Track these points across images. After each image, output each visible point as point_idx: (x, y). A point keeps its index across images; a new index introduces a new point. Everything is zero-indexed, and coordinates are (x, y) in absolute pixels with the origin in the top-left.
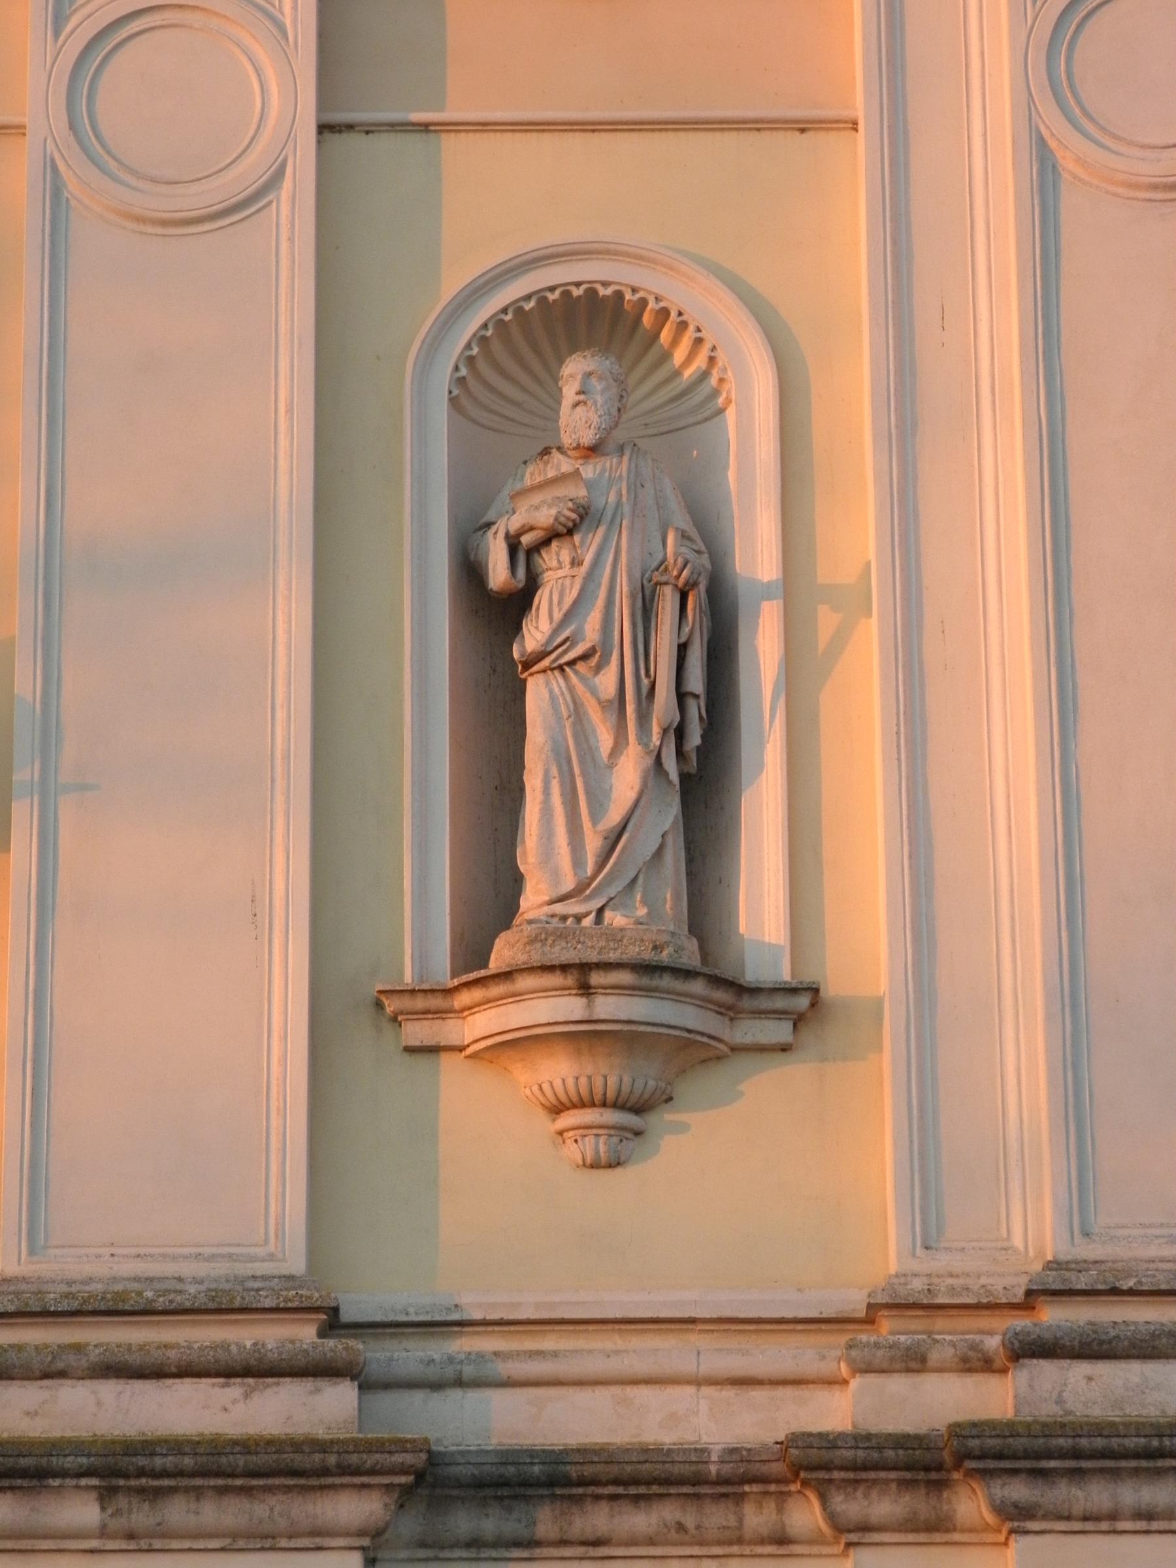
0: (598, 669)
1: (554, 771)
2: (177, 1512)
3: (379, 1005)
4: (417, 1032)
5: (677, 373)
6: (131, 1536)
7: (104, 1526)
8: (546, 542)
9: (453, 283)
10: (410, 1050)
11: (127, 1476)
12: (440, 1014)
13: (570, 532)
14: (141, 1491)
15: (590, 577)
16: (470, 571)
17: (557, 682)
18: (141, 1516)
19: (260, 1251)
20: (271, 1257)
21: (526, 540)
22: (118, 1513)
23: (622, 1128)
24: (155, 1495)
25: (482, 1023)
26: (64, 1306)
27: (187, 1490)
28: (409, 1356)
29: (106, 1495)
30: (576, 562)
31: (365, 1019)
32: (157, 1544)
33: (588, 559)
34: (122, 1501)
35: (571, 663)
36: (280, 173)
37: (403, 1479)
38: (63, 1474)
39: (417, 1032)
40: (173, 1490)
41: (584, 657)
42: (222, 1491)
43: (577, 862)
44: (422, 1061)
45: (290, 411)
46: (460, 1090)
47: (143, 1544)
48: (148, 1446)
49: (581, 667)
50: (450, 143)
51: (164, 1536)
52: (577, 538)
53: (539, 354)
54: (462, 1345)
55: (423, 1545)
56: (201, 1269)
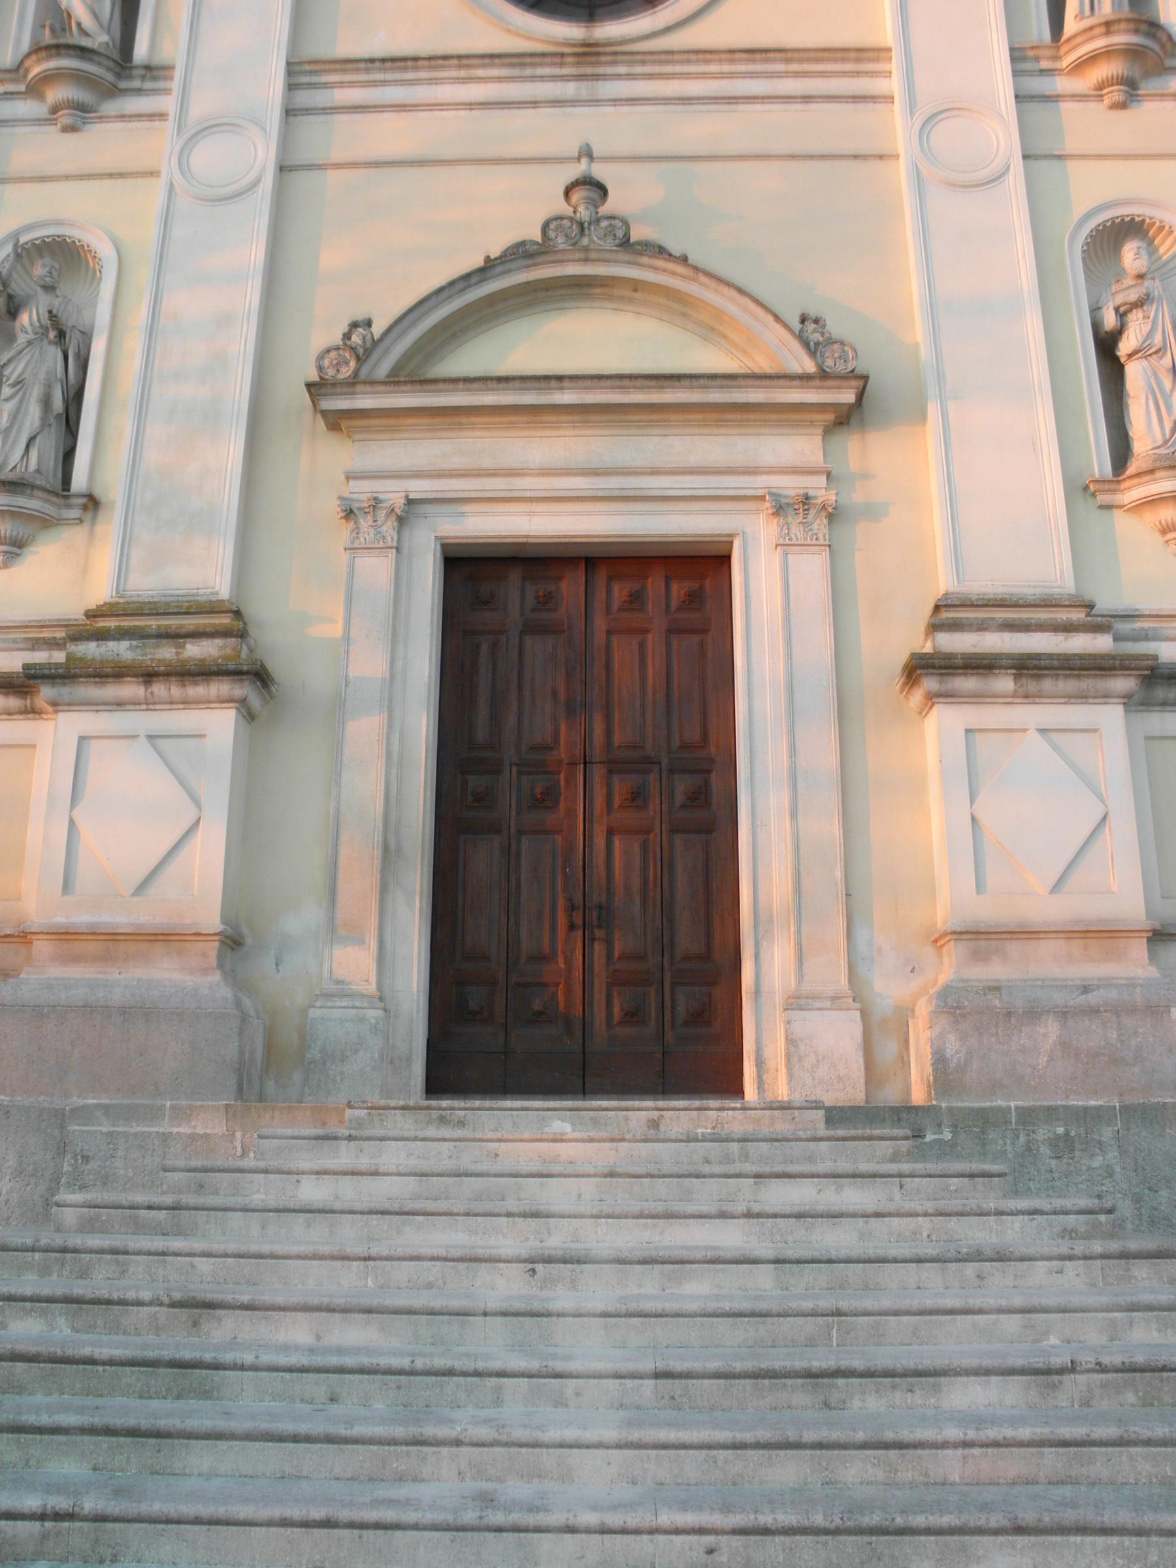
0: (1161, 358)
1: (1150, 396)
2: (1048, 684)
3: (1086, 488)
4: (1103, 498)
5: (1161, 257)
6: (1026, 697)
7: (1016, 691)
8: (1130, 310)
9: (1078, 212)
10: (1101, 507)
11: (1028, 669)
12: (1114, 491)
13: (1142, 305)
14: (1032, 676)
15: (1154, 322)
16: (1096, 326)
17: (1144, 363)
18: (1032, 686)
19: (1055, 584)
20: (1060, 587)
21: (1122, 309)
22: (1022, 686)
23: (6, 552)
24: (1038, 677)
25: (1134, 493)
26: (980, 603)
27: (1052, 676)
28: (1124, 627)
29: (1017, 677)
30: (1146, 317)
31: (1083, 492)
32: (1037, 700)
33: (1152, 315)
34: (1024, 681)
35: (1150, 355)
36: (1008, 168)
37: (1146, 672)
38: (1000, 667)
39: (1103, 498)
40: (1046, 675)
41: (1156, 352)
42: (1067, 676)
43: (1163, 434)
44: (1104, 512)
45: (1024, 255)
46: (1122, 522)
47: (1031, 700)
48: (1038, 656)
49: (1154, 356)
50: (1071, 165)
51: (1041, 697)
52: (1145, 308)
53: (1098, 257)
54: (1138, 625)
55: (1143, 704)
56: (1032, 591)
